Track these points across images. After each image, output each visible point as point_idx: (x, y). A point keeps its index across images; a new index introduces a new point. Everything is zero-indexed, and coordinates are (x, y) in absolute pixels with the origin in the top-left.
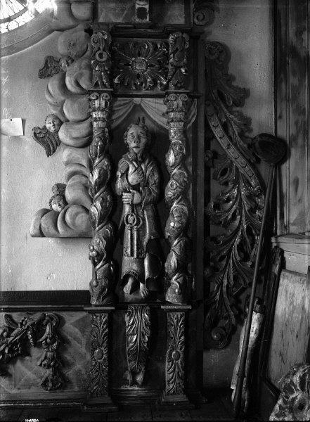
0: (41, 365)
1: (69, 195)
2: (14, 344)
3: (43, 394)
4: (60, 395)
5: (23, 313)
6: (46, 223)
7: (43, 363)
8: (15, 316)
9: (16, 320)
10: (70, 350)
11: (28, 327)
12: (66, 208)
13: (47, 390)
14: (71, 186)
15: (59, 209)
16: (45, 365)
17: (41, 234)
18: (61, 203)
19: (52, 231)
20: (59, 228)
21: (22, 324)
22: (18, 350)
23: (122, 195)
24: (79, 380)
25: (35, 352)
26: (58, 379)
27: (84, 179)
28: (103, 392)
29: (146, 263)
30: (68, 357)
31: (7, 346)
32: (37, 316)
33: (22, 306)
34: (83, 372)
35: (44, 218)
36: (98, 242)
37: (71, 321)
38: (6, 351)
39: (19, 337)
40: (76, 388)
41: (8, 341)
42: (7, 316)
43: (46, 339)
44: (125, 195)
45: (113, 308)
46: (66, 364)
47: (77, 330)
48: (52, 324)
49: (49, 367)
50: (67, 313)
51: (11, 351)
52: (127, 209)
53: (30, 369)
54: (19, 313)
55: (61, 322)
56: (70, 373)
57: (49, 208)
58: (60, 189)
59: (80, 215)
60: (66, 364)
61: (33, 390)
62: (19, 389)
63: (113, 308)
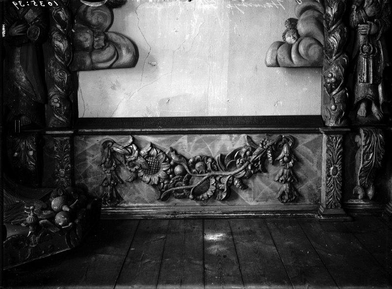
0: (278, 180)
1: (301, 28)
2: (255, 161)
3: (280, 206)
4: (293, 207)
5: (262, 135)
6: (282, 54)
7: (281, 179)
8: (255, 137)
9: (255, 141)
10: (303, 168)
11: (268, 147)
12: (299, 39)
13: (283, 202)
14: (302, 20)
15: (293, 41)
16: (282, 181)
17: (277, 65)
18: (295, 36)
19: (287, 61)
20: (294, 59)
21: (262, 144)
22: (258, 167)
23: (357, 27)
24: (310, 195)
25: (272, 169)
26: (293, 195)
27: (316, 14)
28: (337, 205)
29: (380, 88)
30: (300, 174)
31: (250, 163)
32: (276, 137)
33: (210, 129)
34: (314, 187)
35: (279, 49)
36: (334, 71)
37: (305, 141)
38: (249, 167)
39: (260, 155)
40: (308, 202)
41: (250, 159)
42: (249, 138)
43: (283, 158)
44: (361, 26)
45: (349, 130)
46: (299, 180)
47: (309, 150)
48: (288, 145)
49: (286, 182)
50: (301, 135)
51: (253, 167)
52: (361, 38)
53: (268, 184)
54: (258, 135)
55: (295, 143)
56: (302, 188)
57: (282, 40)
58: (292, 23)
59: (313, 46)
60: (299, 180)
61: (270, 202)
62: (257, 201)
63: (349, 130)
